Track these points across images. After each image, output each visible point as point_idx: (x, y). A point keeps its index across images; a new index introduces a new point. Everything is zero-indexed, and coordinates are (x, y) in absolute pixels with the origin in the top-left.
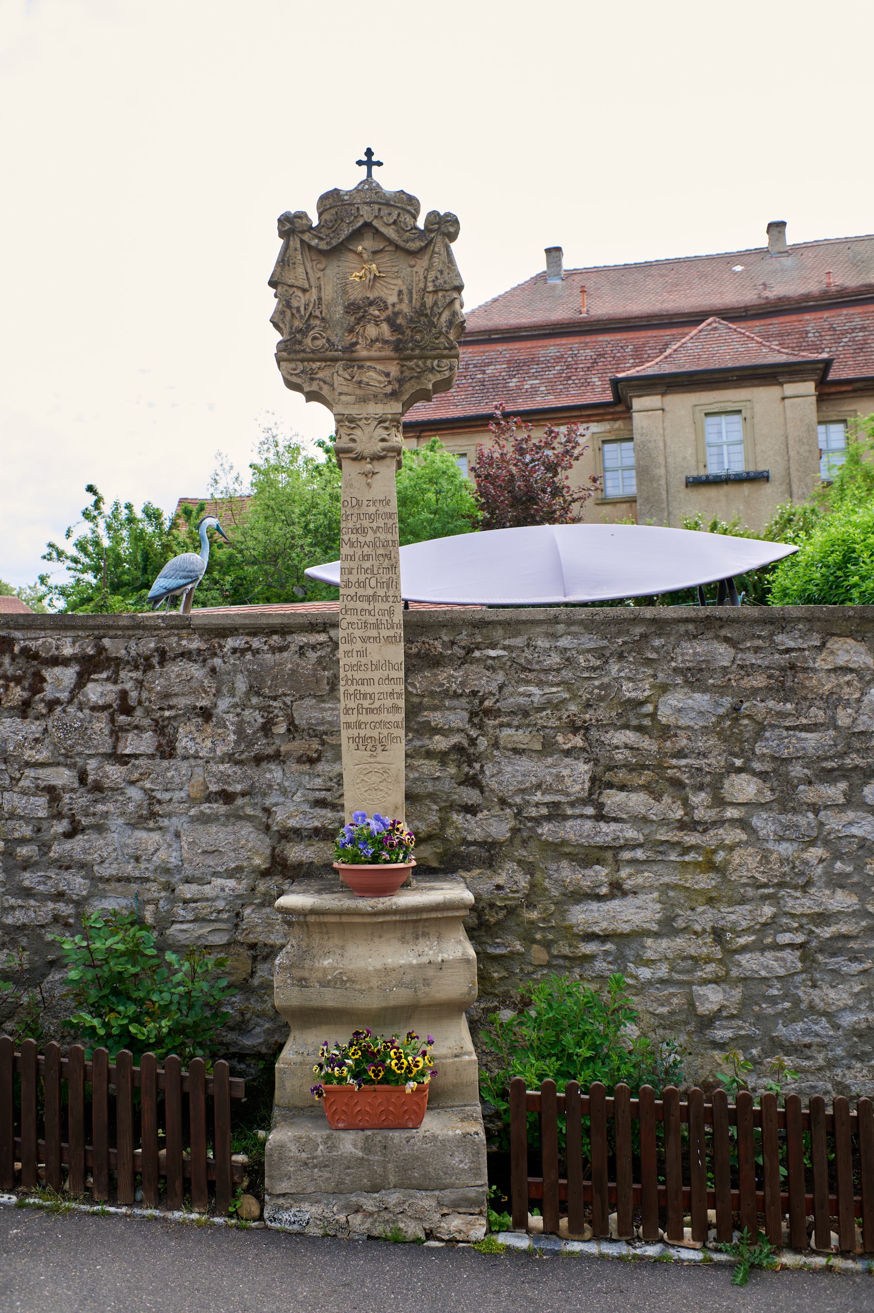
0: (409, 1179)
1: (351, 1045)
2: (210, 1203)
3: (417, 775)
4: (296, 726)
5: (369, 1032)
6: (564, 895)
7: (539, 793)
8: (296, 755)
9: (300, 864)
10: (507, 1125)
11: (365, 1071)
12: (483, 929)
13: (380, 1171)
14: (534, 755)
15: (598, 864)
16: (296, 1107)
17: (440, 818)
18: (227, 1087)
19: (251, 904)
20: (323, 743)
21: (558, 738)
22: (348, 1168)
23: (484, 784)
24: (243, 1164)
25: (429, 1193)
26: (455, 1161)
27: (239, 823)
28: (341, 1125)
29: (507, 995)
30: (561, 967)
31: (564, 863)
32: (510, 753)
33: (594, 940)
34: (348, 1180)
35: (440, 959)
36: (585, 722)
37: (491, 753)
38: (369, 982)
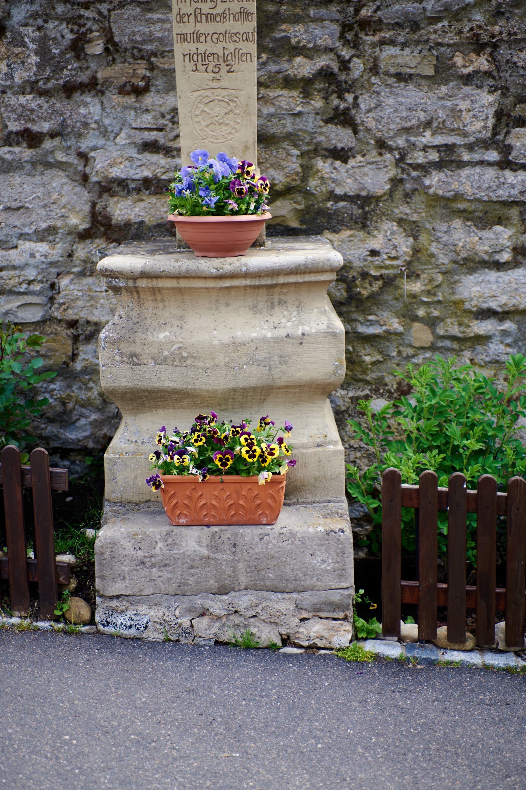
0: (262, 580)
1: (193, 431)
2: (32, 606)
3: (272, 110)
4: (115, 45)
5: (214, 416)
6: (455, 262)
7: (428, 133)
8: (117, 83)
9: (128, 225)
10: (378, 527)
11: (211, 460)
12: (354, 304)
13: (229, 571)
14: (423, 82)
15: (499, 223)
16: (129, 502)
17: (302, 166)
18: (48, 478)
19: (69, 273)
20: (152, 67)
21: (456, 59)
22: (192, 567)
23: (358, 121)
24: (69, 564)
25: (285, 595)
26: (316, 561)
27: (50, 173)
28: (183, 521)
29: (380, 382)
30: (448, 349)
31: (457, 223)
32: (391, 81)
33: (489, 317)
34: (191, 581)
35: (300, 332)
36: (493, 36)
37: (368, 80)
38: (213, 359)
